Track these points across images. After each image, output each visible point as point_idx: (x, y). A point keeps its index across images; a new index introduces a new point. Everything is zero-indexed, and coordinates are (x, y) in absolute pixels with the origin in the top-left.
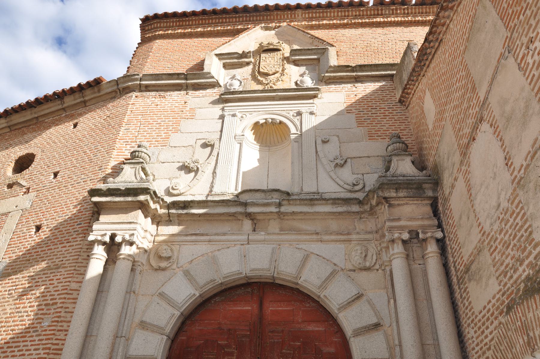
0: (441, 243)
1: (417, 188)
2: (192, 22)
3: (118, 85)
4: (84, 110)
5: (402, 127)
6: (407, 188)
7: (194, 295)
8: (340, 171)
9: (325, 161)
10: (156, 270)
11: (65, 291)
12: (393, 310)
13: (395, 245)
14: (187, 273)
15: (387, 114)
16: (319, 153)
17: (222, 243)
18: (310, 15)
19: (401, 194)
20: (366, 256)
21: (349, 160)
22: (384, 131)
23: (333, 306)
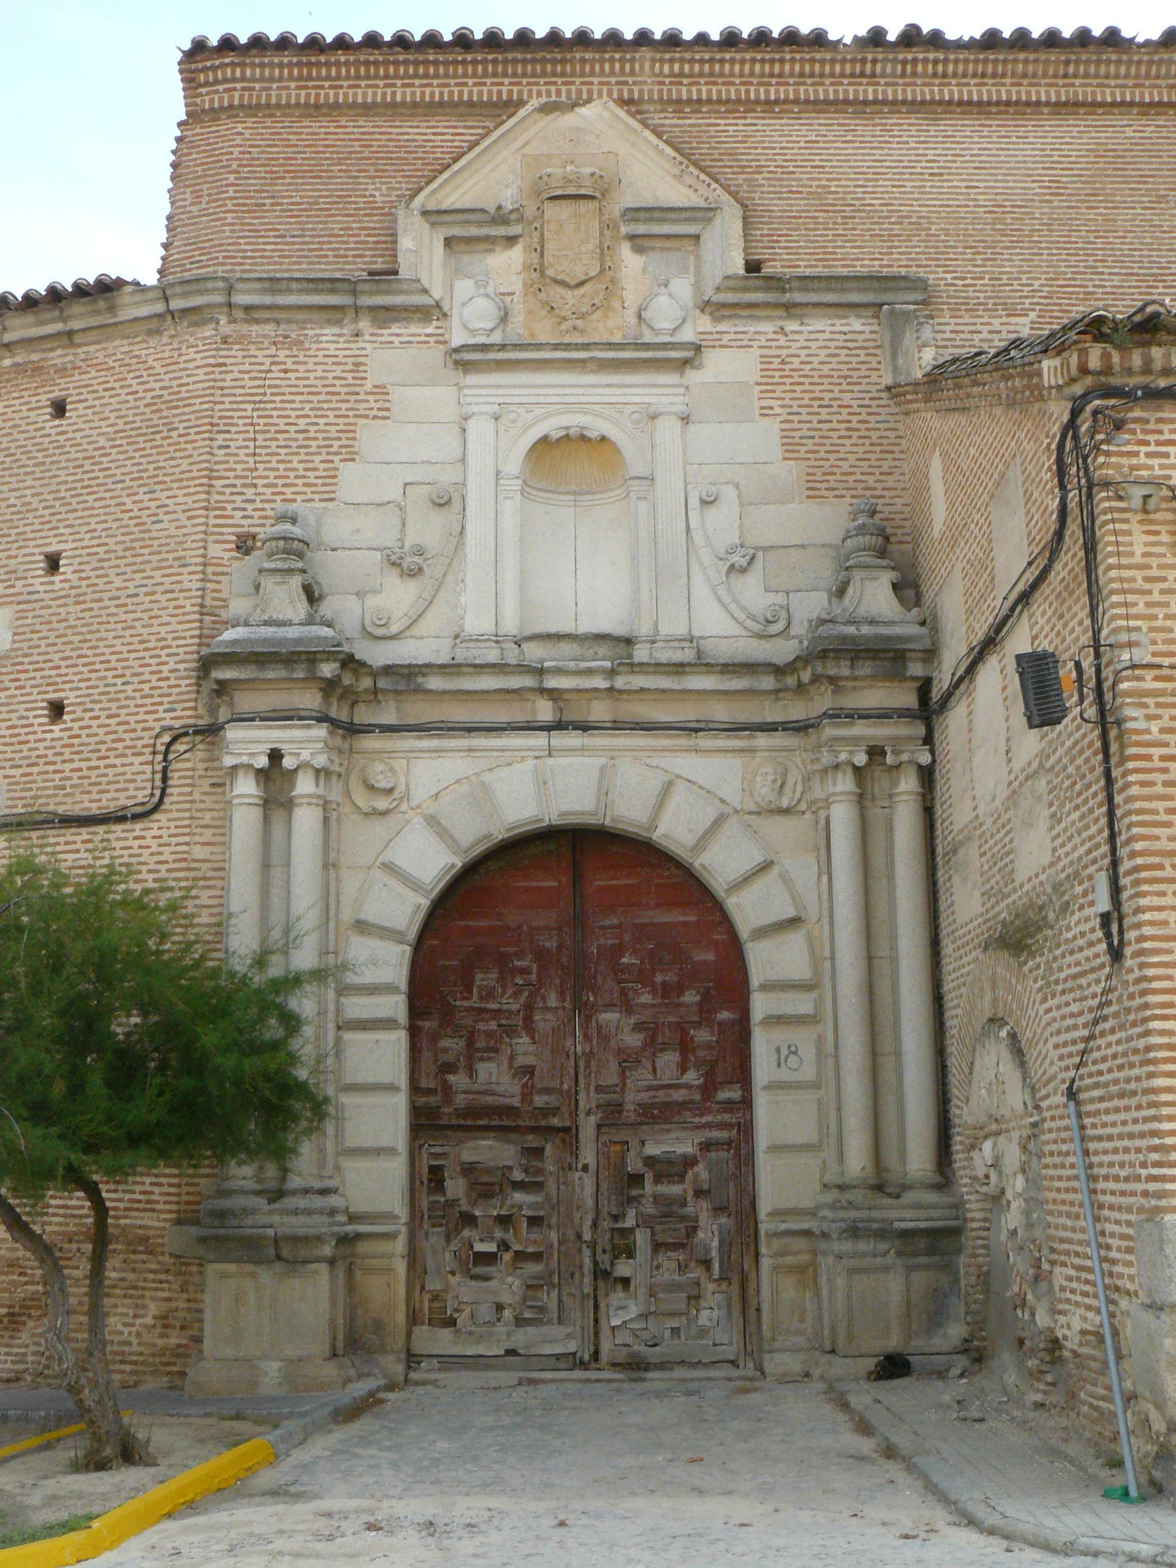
0: (927, 776)
1: (894, 659)
2: (339, 72)
3: (167, 300)
4: (70, 358)
5: (886, 466)
6: (874, 659)
7: (453, 865)
8: (738, 582)
9: (706, 555)
10: (367, 814)
11: (183, 865)
12: (825, 896)
13: (840, 775)
14: (432, 821)
15: (854, 425)
16: (693, 534)
17: (496, 754)
18: (676, 67)
19: (860, 672)
20: (782, 785)
21: (760, 554)
22: (843, 474)
23: (719, 882)
